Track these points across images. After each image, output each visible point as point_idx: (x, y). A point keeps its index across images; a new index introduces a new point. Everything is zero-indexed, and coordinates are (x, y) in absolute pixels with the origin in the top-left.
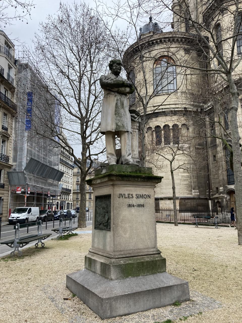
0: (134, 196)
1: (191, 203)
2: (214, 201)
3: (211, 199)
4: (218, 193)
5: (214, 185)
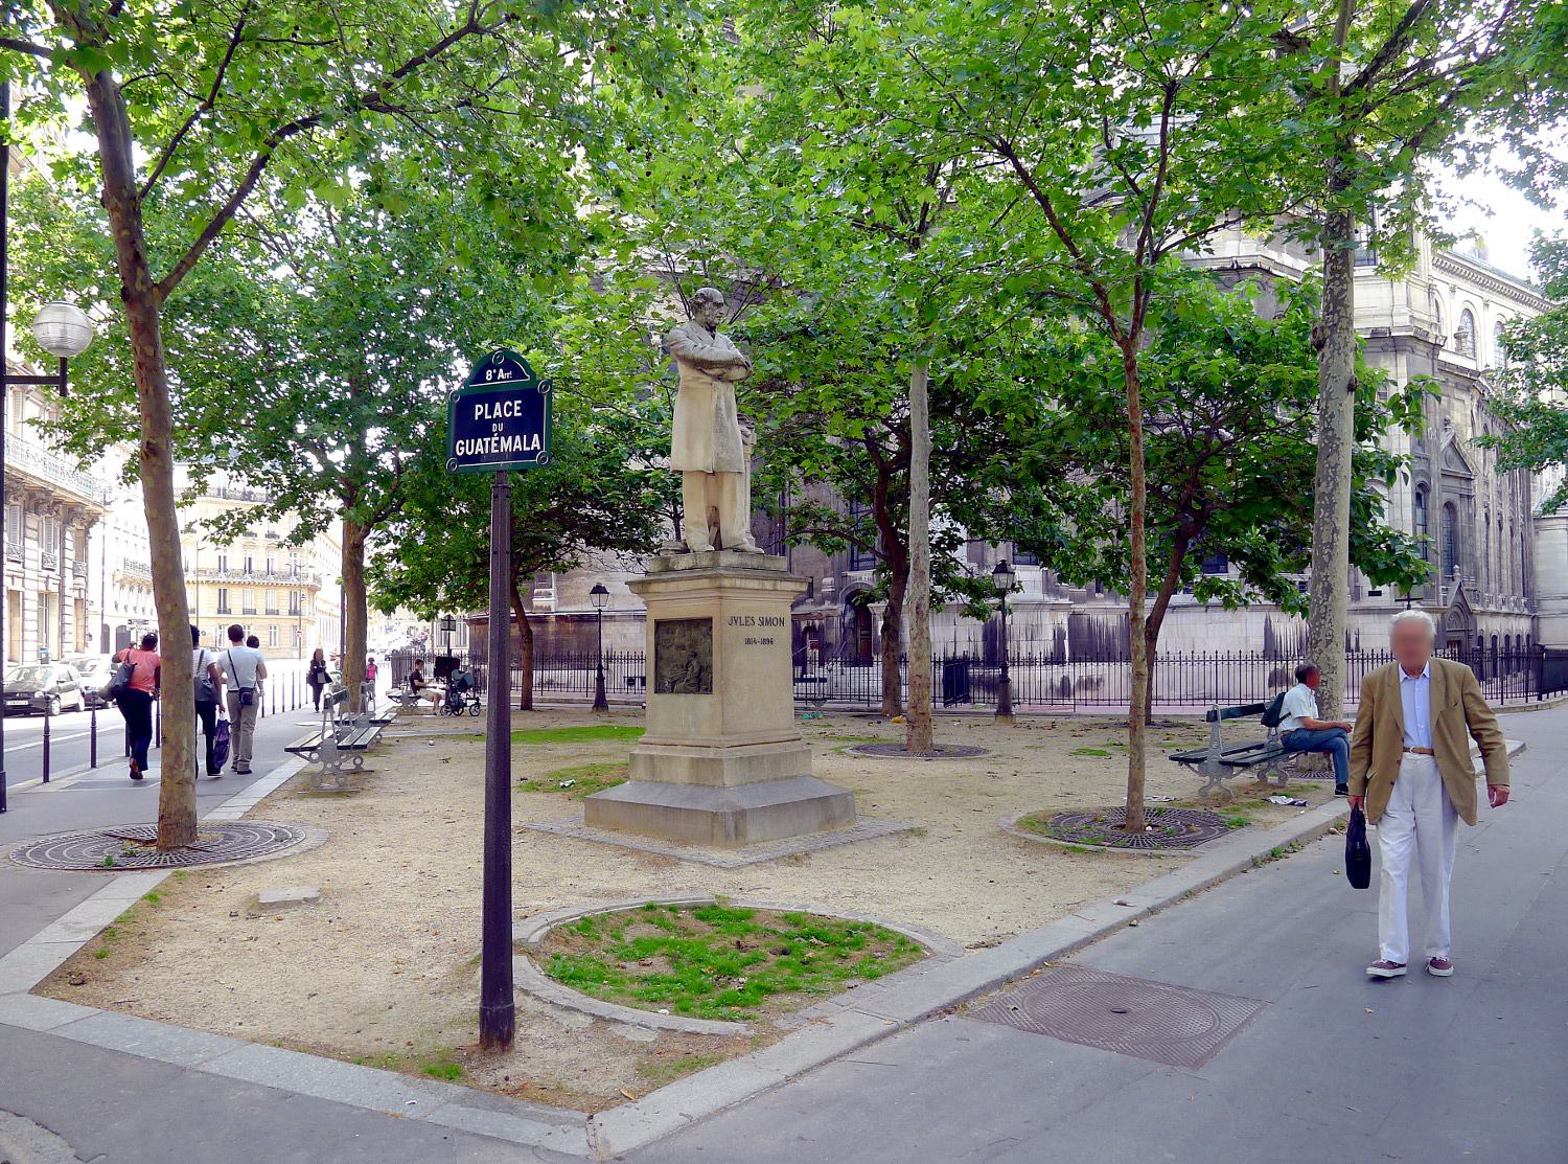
0: (757, 621)
4: (811, 596)
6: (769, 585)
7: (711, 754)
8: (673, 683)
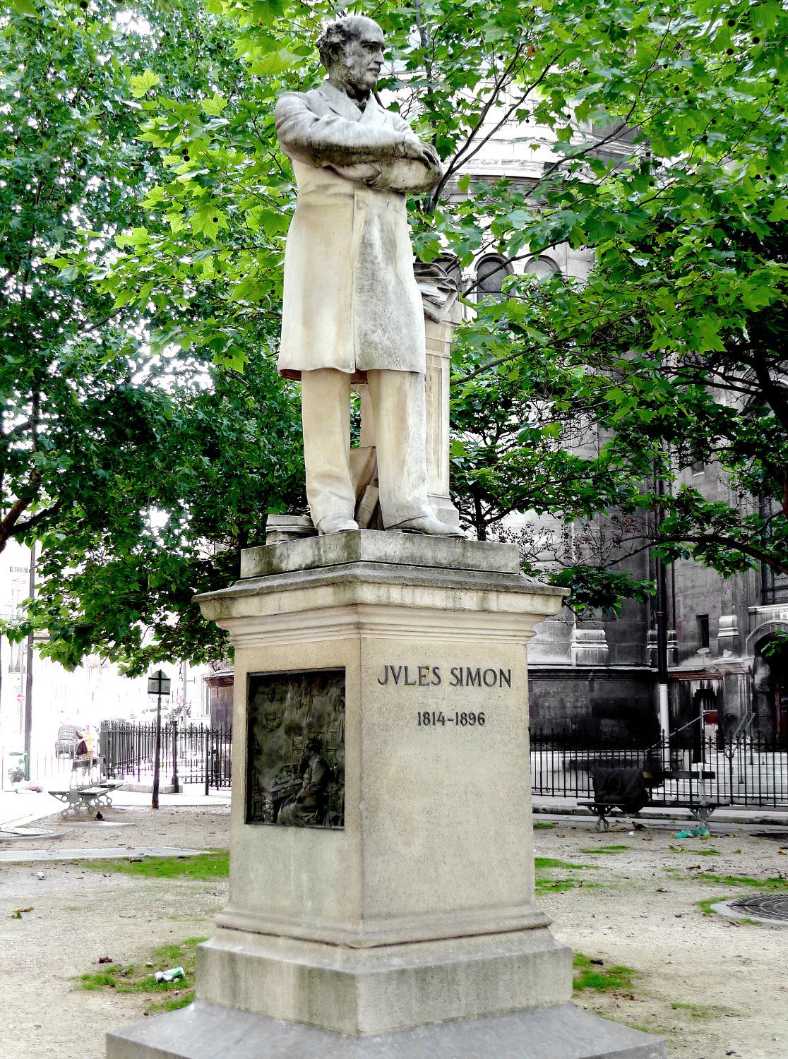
0: (446, 676)
1: (562, 701)
2: (685, 691)
3: (670, 680)
4: (705, 644)
5: (689, 602)
6: (469, 600)
7: (336, 961)
8: (277, 804)
